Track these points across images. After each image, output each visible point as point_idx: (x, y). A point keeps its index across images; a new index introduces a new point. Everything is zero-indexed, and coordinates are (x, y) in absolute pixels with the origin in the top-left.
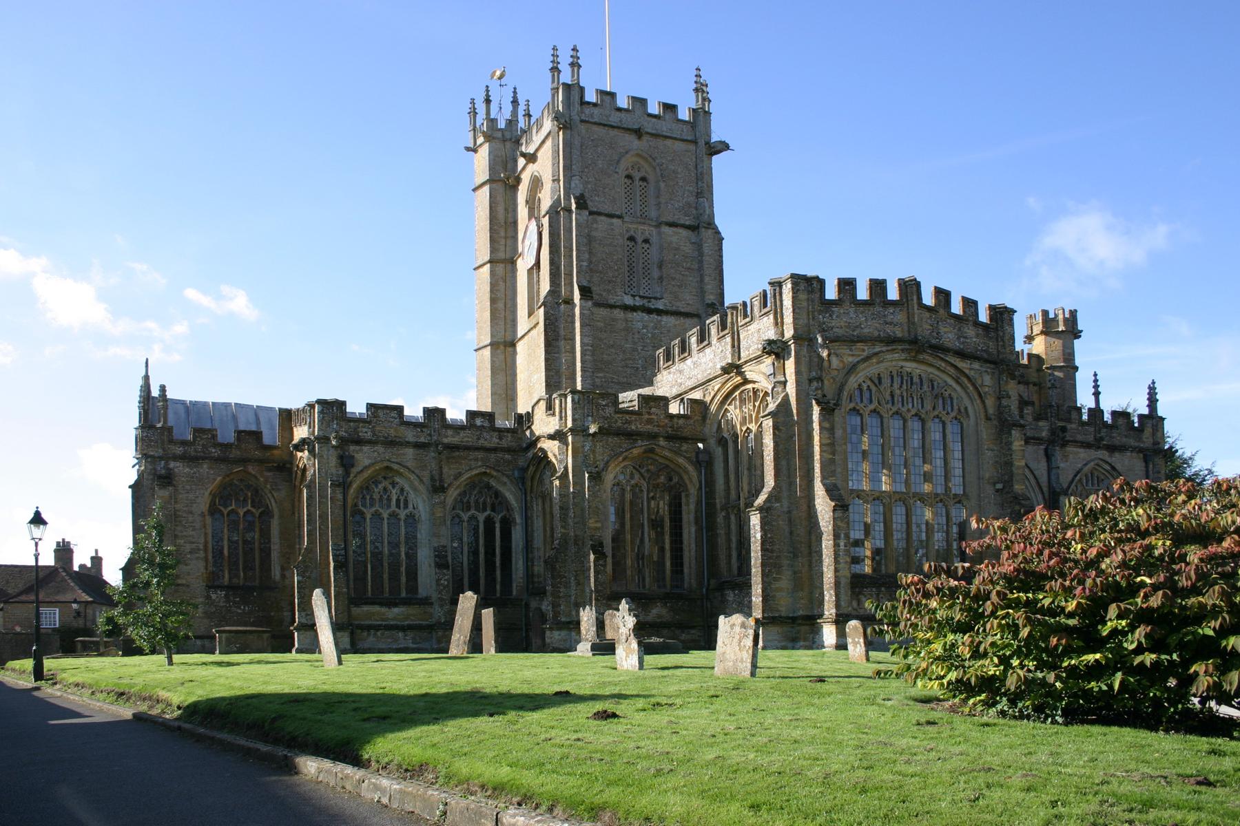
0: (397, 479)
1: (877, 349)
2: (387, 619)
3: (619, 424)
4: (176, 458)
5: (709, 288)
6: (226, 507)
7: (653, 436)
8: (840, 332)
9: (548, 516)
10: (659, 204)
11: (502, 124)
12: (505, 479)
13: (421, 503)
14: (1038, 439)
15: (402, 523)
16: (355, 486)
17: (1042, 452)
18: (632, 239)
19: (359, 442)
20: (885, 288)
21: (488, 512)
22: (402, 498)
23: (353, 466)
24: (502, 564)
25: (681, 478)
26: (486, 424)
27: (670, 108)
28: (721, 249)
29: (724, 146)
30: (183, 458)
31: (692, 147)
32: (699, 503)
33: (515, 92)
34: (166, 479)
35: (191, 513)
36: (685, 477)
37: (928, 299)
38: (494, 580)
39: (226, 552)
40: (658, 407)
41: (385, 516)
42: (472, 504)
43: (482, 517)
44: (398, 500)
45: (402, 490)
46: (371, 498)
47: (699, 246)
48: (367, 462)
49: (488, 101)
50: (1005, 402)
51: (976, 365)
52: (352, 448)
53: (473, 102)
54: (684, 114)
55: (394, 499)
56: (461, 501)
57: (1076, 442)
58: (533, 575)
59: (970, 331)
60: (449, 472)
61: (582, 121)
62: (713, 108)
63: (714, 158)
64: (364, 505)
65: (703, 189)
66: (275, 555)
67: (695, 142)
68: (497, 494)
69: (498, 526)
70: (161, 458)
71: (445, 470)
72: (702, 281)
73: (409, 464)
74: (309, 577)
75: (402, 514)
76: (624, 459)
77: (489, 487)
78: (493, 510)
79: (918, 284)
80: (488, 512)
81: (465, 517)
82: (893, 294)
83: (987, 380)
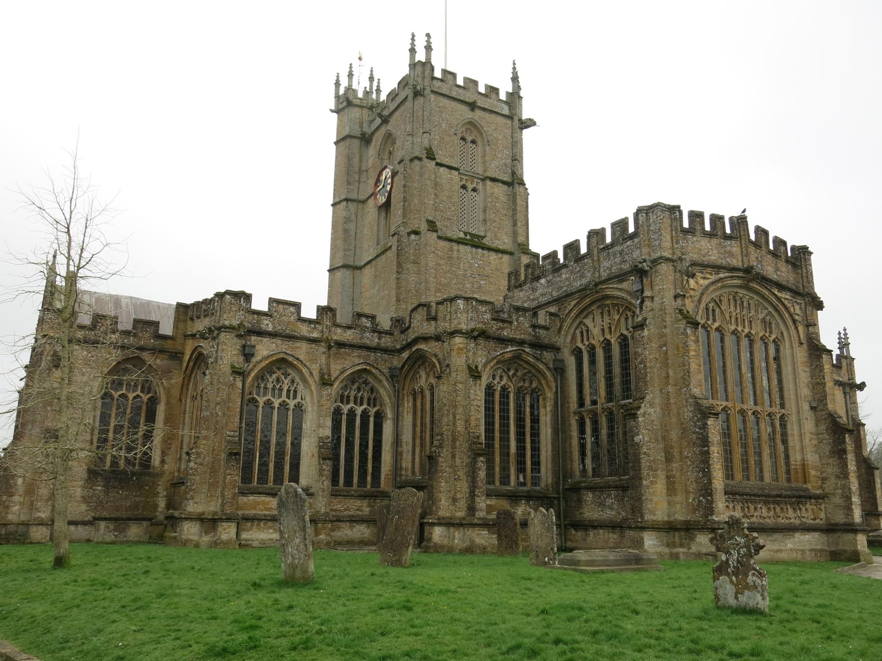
0: (290, 371)
1: (722, 275)
7: (522, 343)
9: (419, 413)
10: (484, 162)
15: (290, 413)
16: (253, 375)
18: (464, 187)
19: (261, 333)
24: (373, 457)
25: (540, 382)
26: (369, 325)
27: (493, 90)
29: (531, 123)
31: (509, 122)
32: (556, 405)
33: (372, 71)
36: (543, 382)
38: (366, 471)
41: (276, 405)
42: (352, 398)
43: (359, 410)
44: (288, 391)
45: (293, 381)
46: (266, 388)
47: (513, 198)
48: (266, 353)
49: (350, 75)
52: (253, 338)
54: (503, 96)
55: (285, 388)
58: (401, 469)
61: (432, 91)
63: (525, 131)
65: (516, 159)
67: (510, 117)
73: (302, 357)
74: (201, 464)
75: (292, 403)
76: (497, 363)
77: (366, 383)
78: (369, 405)
80: (365, 406)
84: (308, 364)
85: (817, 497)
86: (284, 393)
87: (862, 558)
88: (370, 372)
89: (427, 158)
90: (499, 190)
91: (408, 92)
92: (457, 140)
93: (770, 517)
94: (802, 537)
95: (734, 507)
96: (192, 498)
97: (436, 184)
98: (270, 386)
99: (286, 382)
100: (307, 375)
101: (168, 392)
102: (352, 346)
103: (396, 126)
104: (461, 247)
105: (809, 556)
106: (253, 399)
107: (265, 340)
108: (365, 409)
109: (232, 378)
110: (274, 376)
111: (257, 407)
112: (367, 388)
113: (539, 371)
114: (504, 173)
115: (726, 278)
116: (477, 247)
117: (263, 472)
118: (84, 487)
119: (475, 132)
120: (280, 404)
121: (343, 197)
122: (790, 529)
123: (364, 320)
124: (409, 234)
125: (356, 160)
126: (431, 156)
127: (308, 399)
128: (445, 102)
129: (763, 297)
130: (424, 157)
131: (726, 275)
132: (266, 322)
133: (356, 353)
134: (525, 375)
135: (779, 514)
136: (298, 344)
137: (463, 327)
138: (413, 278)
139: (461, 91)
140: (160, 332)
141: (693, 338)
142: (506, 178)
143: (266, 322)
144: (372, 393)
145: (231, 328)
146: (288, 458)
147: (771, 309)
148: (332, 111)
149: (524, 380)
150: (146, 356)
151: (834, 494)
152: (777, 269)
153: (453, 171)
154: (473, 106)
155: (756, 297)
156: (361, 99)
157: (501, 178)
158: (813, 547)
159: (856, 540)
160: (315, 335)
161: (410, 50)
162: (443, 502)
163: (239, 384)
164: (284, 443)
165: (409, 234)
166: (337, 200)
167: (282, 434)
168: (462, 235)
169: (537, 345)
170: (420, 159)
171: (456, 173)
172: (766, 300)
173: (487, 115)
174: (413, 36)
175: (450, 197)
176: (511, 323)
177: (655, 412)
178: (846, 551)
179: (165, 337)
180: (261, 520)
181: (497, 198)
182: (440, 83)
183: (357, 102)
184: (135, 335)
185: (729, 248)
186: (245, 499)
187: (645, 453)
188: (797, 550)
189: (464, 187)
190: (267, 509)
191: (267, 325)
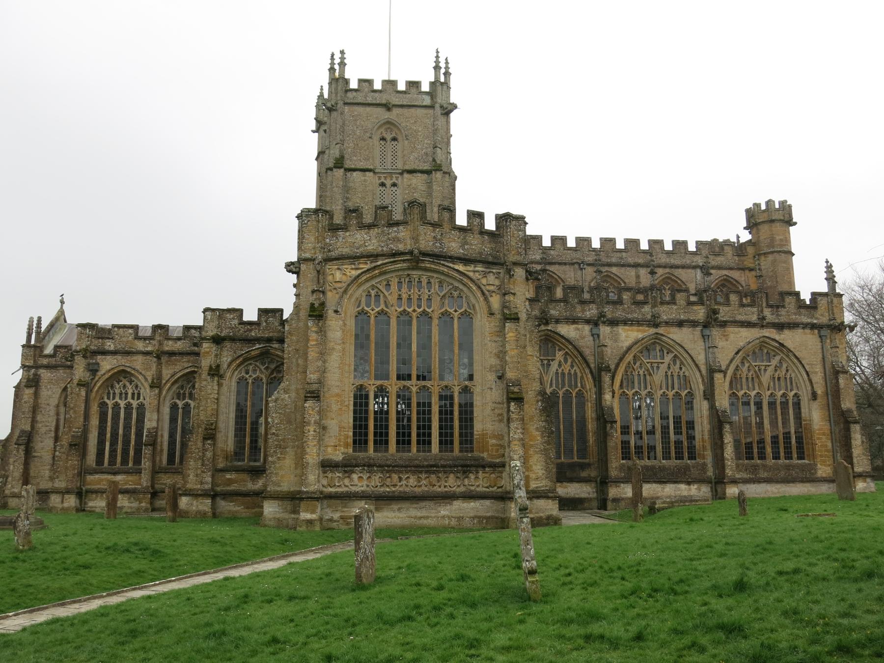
1: (379, 263)
8: (346, 251)
18: (383, 185)
19: (104, 353)
22: (136, 392)
27: (414, 85)
28: (454, 189)
30: (47, 367)
31: (431, 111)
40: (274, 317)
43: (122, 404)
44: (133, 394)
46: (114, 394)
48: (108, 367)
51: (480, 268)
52: (99, 357)
54: (425, 87)
60: (167, 373)
62: (452, 84)
67: (432, 107)
70: (32, 367)
73: (138, 367)
75: (135, 403)
76: (245, 360)
83: (491, 279)
84: (143, 372)
85: (493, 466)
86: (130, 395)
94: (465, 505)
98: (117, 391)
102: (182, 354)
105: (467, 523)
107: (108, 357)
114: (425, 162)
119: (395, 130)
122: (448, 497)
123: (193, 331)
128: (360, 109)
133: (185, 359)
136: (135, 358)
142: (426, 167)
147: (456, 284)
153: (367, 173)
154: (388, 107)
155: (435, 276)
157: (421, 168)
158: (479, 514)
160: (149, 349)
161: (329, 70)
162: (191, 477)
163: (83, 393)
167: (127, 427)
171: (371, 174)
172: (448, 275)
173: (405, 110)
175: (363, 198)
177: (289, 397)
182: (354, 94)
185: (393, 235)
186: (92, 477)
187: (274, 434)
188: (449, 517)
189: (383, 185)
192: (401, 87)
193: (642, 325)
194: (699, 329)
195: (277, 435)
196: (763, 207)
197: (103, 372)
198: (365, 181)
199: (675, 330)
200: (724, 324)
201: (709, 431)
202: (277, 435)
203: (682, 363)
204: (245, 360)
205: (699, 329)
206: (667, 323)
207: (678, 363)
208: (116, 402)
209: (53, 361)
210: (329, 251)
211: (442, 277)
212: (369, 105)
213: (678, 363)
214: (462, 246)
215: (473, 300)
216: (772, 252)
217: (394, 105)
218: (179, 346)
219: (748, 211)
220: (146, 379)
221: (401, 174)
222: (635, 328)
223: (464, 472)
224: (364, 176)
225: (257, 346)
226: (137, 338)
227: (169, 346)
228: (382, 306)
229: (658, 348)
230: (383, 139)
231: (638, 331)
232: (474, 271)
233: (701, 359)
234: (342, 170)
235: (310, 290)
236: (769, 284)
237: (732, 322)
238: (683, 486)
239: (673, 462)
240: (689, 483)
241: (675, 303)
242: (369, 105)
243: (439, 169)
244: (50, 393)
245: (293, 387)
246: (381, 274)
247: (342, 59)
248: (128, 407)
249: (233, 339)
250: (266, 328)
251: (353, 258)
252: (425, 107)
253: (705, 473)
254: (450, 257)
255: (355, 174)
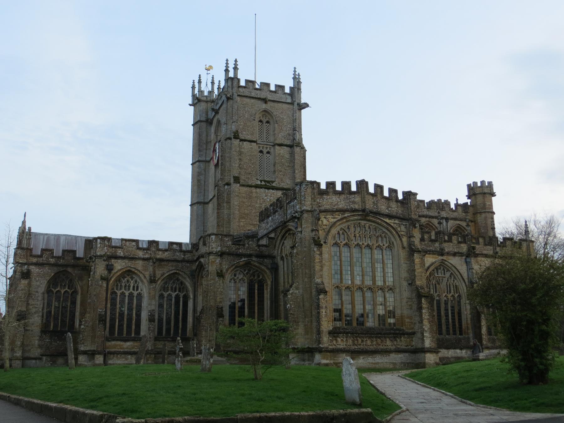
0: (134, 276)
1: (346, 215)
2: (123, 348)
3: (234, 249)
4: (32, 264)
5: (297, 176)
6: (55, 289)
7: (250, 256)
8: (328, 207)
10: (274, 134)
11: (206, 94)
12: (185, 276)
13: (145, 289)
14: (461, 253)
15: (135, 298)
16: (113, 279)
17: (464, 260)
18: (261, 152)
19: (117, 258)
20: (350, 185)
21: (169, 292)
22: (136, 285)
23: (112, 270)
25: (263, 276)
27: (280, 88)
29: (306, 105)
30: (36, 264)
31: (291, 106)
32: (272, 289)
33: (213, 78)
34: (26, 275)
35: (37, 292)
36: (266, 276)
37: (372, 190)
38: (178, 327)
39: (53, 312)
42: (170, 288)
43: (174, 295)
44: (134, 287)
45: (136, 281)
46: (121, 286)
47: (292, 154)
48: (119, 268)
49: (200, 82)
50: (412, 239)
51: (397, 221)
52: (113, 260)
53: (194, 82)
54: (287, 90)
56: (164, 287)
57: (482, 254)
59: (394, 205)
60: (158, 273)
63: (302, 111)
64: (117, 289)
65: (296, 128)
66: (77, 314)
67: (292, 103)
68: (182, 283)
69: (181, 299)
71: (157, 272)
72: (294, 172)
73: (139, 269)
74: (87, 326)
75: (135, 293)
76: (236, 267)
77: (178, 279)
78: (180, 291)
79: (367, 183)
81: (166, 294)
82: (354, 188)
83: (403, 228)
85: (408, 334)
86: (131, 288)
87: (427, 366)
88: (178, 274)
89: (234, 138)
90: (284, 151)
91: (224, 98)
92: (256, 123)
93: (373, 345)
94: (396, 356)
95: (347, 340)
96: (83, 344)
97: (241, 153)
98: (123, 285)
99: (132, 282)
100: (143, 278)
101: (82, 288)
102: (168, 261)
103: (222, 116)
104: (258, 190)
106: (115, 292)
107: (119, 261)
108: (178, 294)
109: (101, 282)
110: (126, 279)
111: (117, 296)
112: (179, 282)
113: (263, 270)
114: (288, 140)
115: (348, 216)
116: (268, 189)
117: (168, 330)
118: (39, 340)
120: (129, 294)
121: (197, 160)
123: (175, 246)
124: (225, 185)
125: (204, 135)
126: (236, 136)
127: (144, 290)
129: (378, 223)
130: (232, 137)
131: (349, 215)
132: (119, 252)
134: (254, 272)
135: (380, 343)
137: (215, 250)
138: (226, 212)
139: (258, 92)
140: (77, 256)
141: (318, 253)
142: (288, 142)
143: (119, 252)
144: (182, 285)
145: (101, 256)
146: (134, 322)
147: (384, 230)
148: (190, 105)
149: (254, 276)
150: (69, 270)
151: (418, 332)
152: (388, 207)
153: (253, 143)
154: (265, 101)
155: (373, 224)
156: (206, 97)
158: (403, 361)
159: (425, 357)
160: (147, 256)
162: (203, 342)
163: (105, 285)
164: (132, 314)
165: (225, 185)
166: (194, 161)
167: (130, 309)
168: (259, 183)
169: (261, 256)
170: (230, 139)
171: (255, 144)
174: (227, 60)
176: (244, 245)
178: (421, 363)
179: (79, 259)
180: (118, 354)
181: (283, 157)
182: (244, 89)
183: (205, 99)
184: (63, 259)
186: (110, 343)
187: (291, 314)
189: (261, 152)
190: (121, 348)
191: (120, 253)
192: (273, 88)
193: (435, 254)
194: (464, 257)
195: (294, 315)
196: (479, 185)
197: (115, 271)
198: (252, 148)
199: (451, 257)
200: (476, 256)
201: (471, 319)
202: (294, 315)
203: (455, 278)
204: (236, 267)
205: (464, 257)
206: (448, 254)
207: (452, 278)
208: (123, 292)
209: (40, 260)
210: (319, 207)
211: (377, 225)
212: (253, 98)
213: (452, 278)
214: (387, 208)
215: (393, 239)
216: (485, 212)
217: (270, 100)
218: (166, 255)
219: (469, 186)
220: (145, 277)
221: (274, 146)
222: (431, 256)
223: (394, 338)
224: (251, 145)
225: (243, 259)
226: (139, 248)
227: (160, 255)
228: (346, 241)
229: (442, 269)
230: (261, 121)
231: (433, 258)
232: (394, 223)
233: (465, 276)
234: (239, 140)
235: (310, 229)
236: (483, 231)
237: (480, 254)
238: (458, 351)
239: (451, 337)
240: (461, 349)
241: (452, 242)
242: (253, 98)
243: (295, 146)
244: (38, 283)
245: (301, 286)
246: (347, 221)
247: (236, 65)
248: (131, 295)
249: (229, 254)
250: (248, 248)
251: (332, 212)
252: (288, 103)
253: (469, 343)
254: (383, 214)
255: (245, 143)
